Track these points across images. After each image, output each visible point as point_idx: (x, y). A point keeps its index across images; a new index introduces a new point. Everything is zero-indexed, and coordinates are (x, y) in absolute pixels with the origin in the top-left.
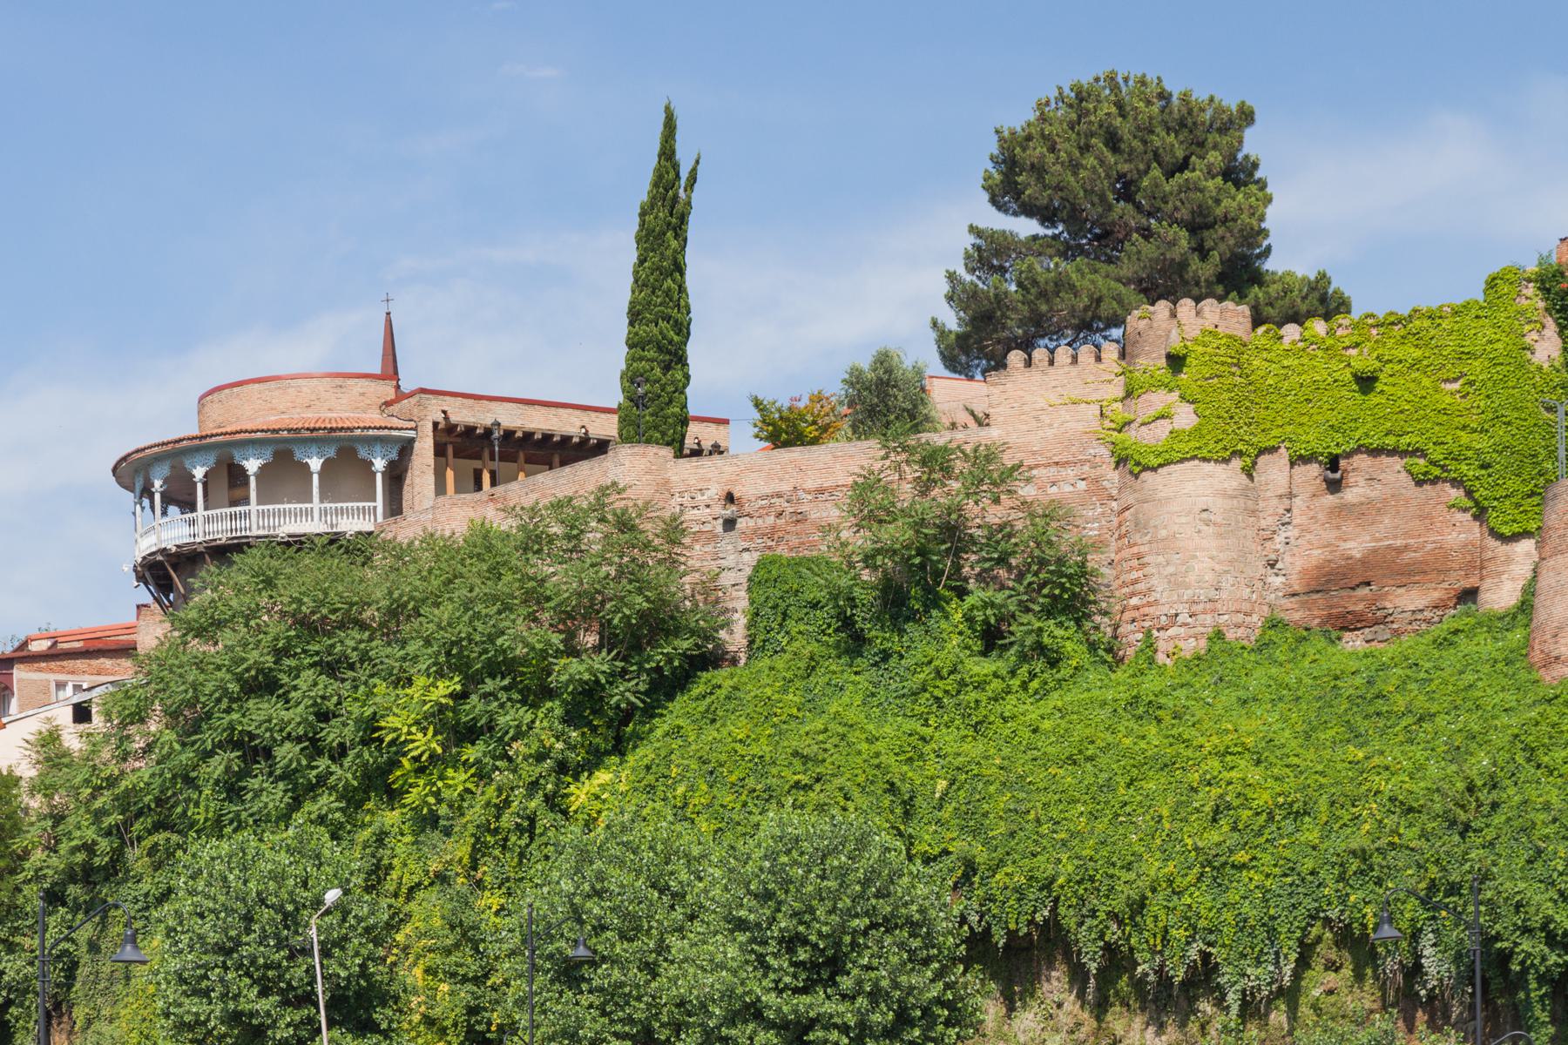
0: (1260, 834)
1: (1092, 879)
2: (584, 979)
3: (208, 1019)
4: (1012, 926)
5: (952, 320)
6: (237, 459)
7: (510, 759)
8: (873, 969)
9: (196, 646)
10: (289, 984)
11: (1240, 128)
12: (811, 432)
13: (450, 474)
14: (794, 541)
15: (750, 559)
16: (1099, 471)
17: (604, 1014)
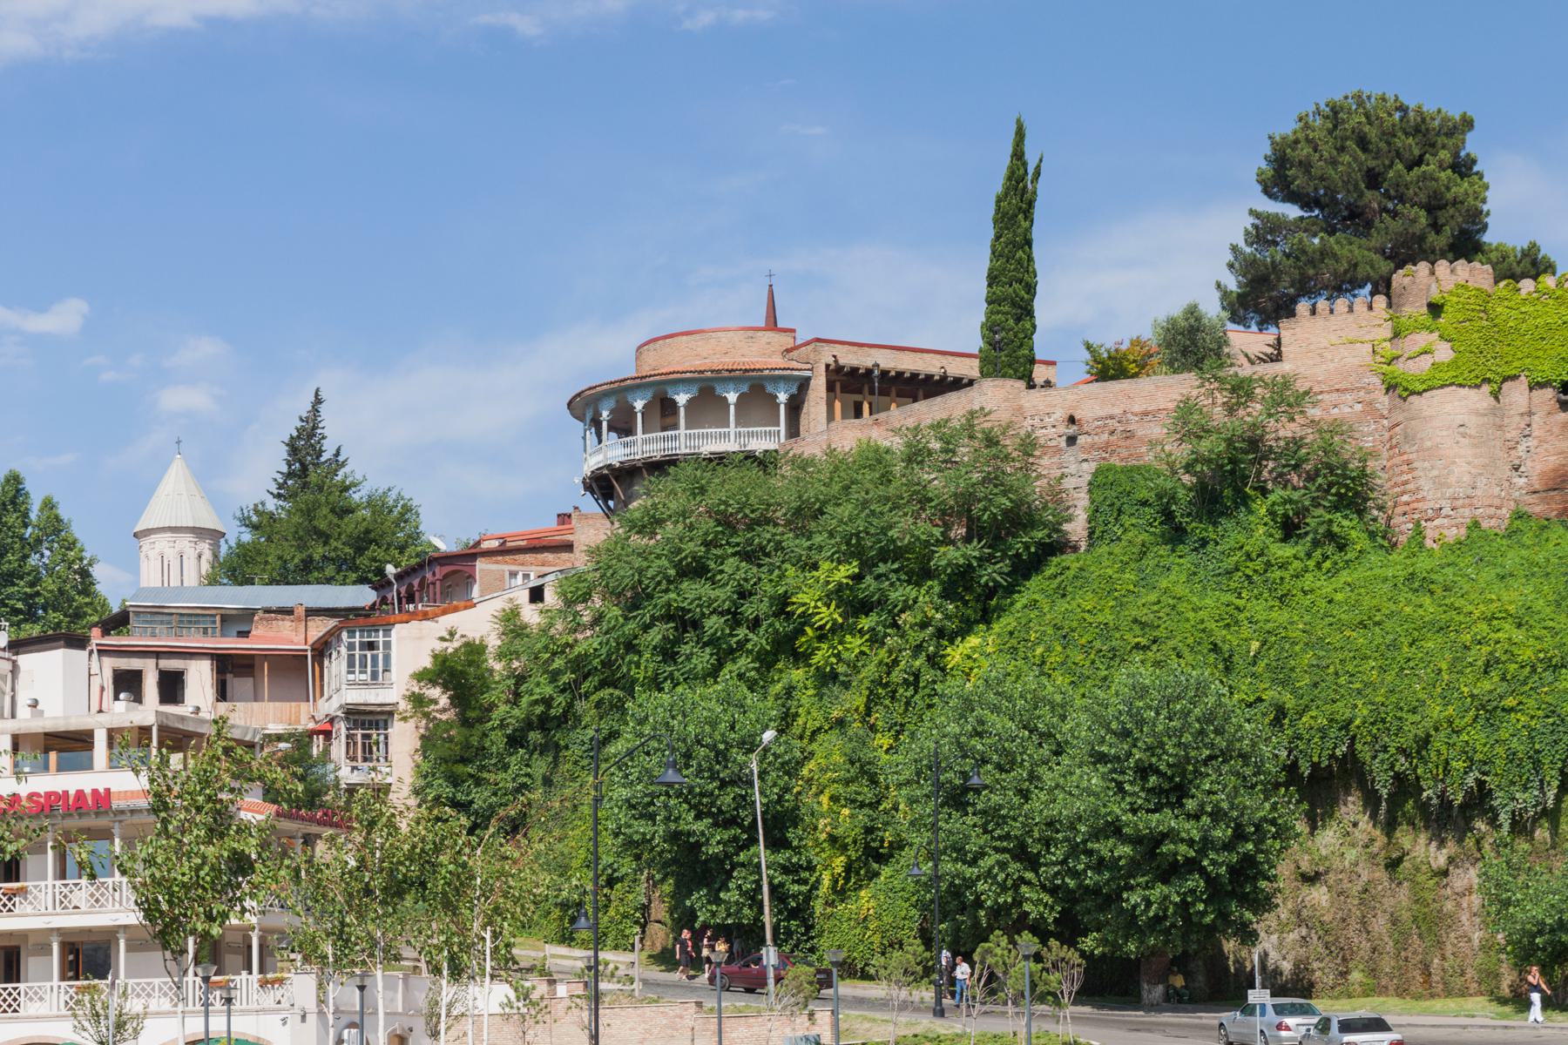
0: (1525, 683)
1: (1383, 721)
2: (968, 804)
3: (653, 838)
4: (1315, 759)
5: (1232, 283)
6: (670, 394)
7: (898, 627)
8: (1214, 793)
9: (637, 541)
10: (719, 809)
11: (1463, 133)
12: (1133, 368)
13: (838, 405)
14: (1124, 453)
15: (1090, 467)
16: (1372, 396)
17: (986, 832)
